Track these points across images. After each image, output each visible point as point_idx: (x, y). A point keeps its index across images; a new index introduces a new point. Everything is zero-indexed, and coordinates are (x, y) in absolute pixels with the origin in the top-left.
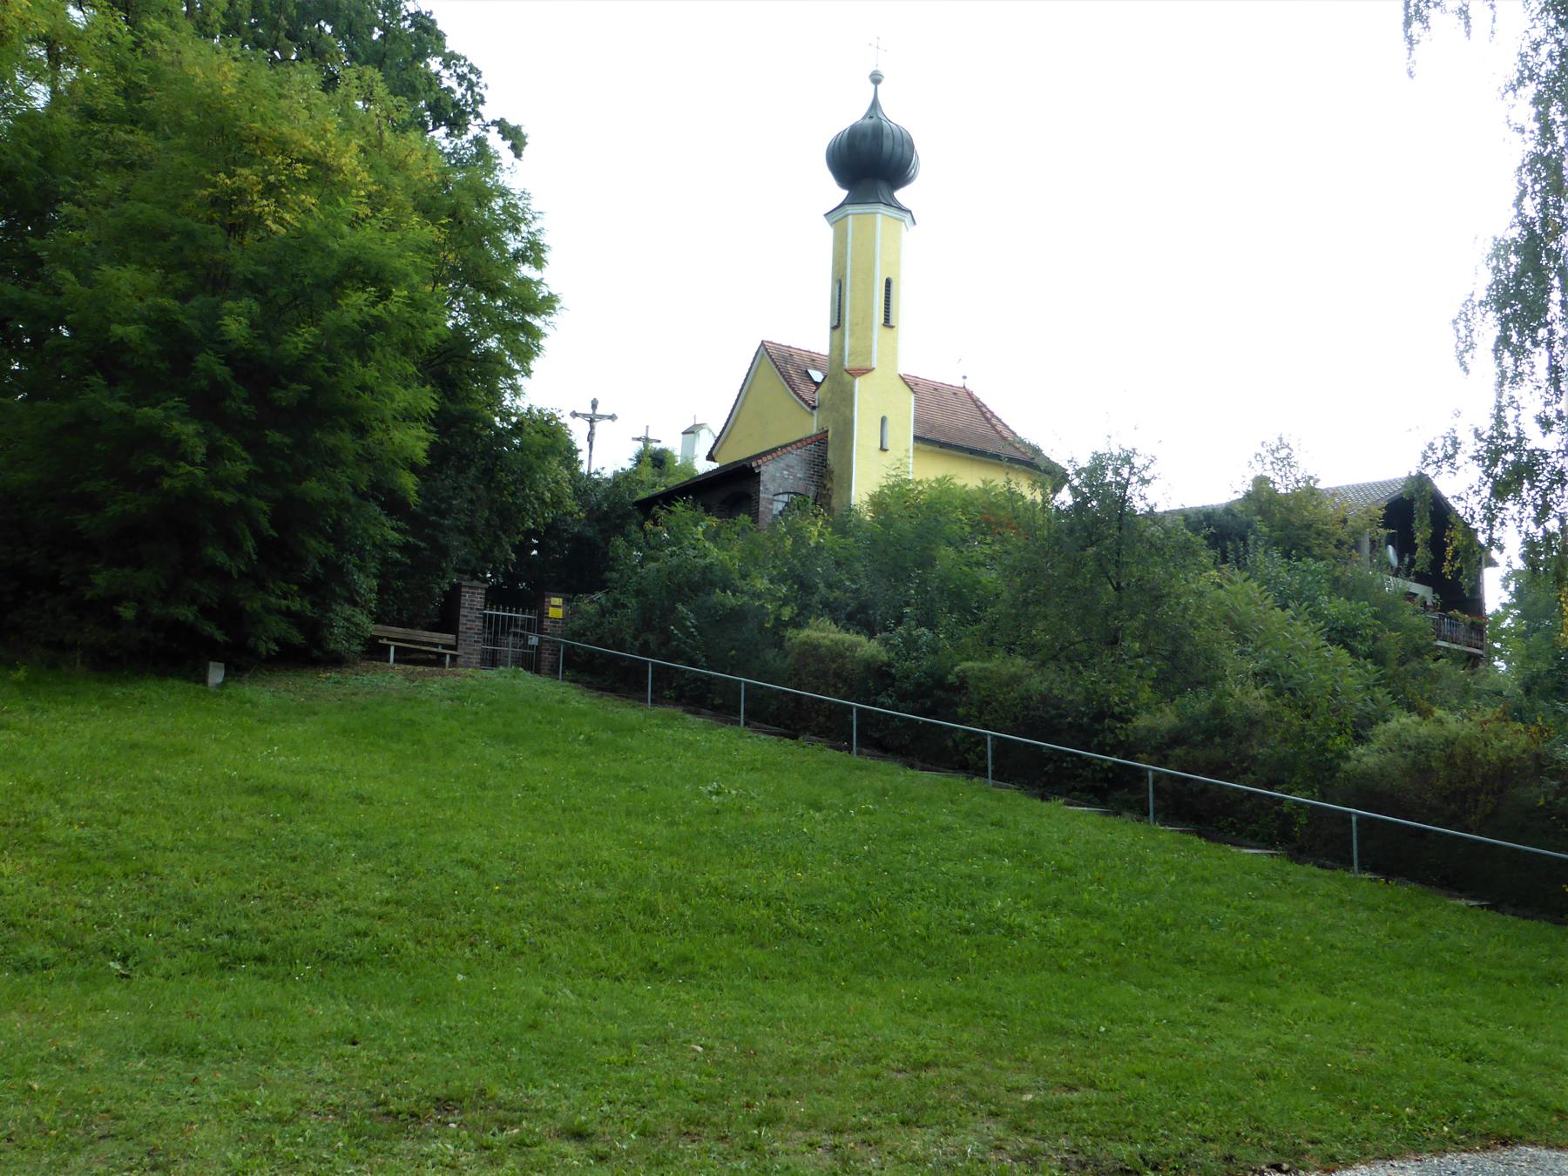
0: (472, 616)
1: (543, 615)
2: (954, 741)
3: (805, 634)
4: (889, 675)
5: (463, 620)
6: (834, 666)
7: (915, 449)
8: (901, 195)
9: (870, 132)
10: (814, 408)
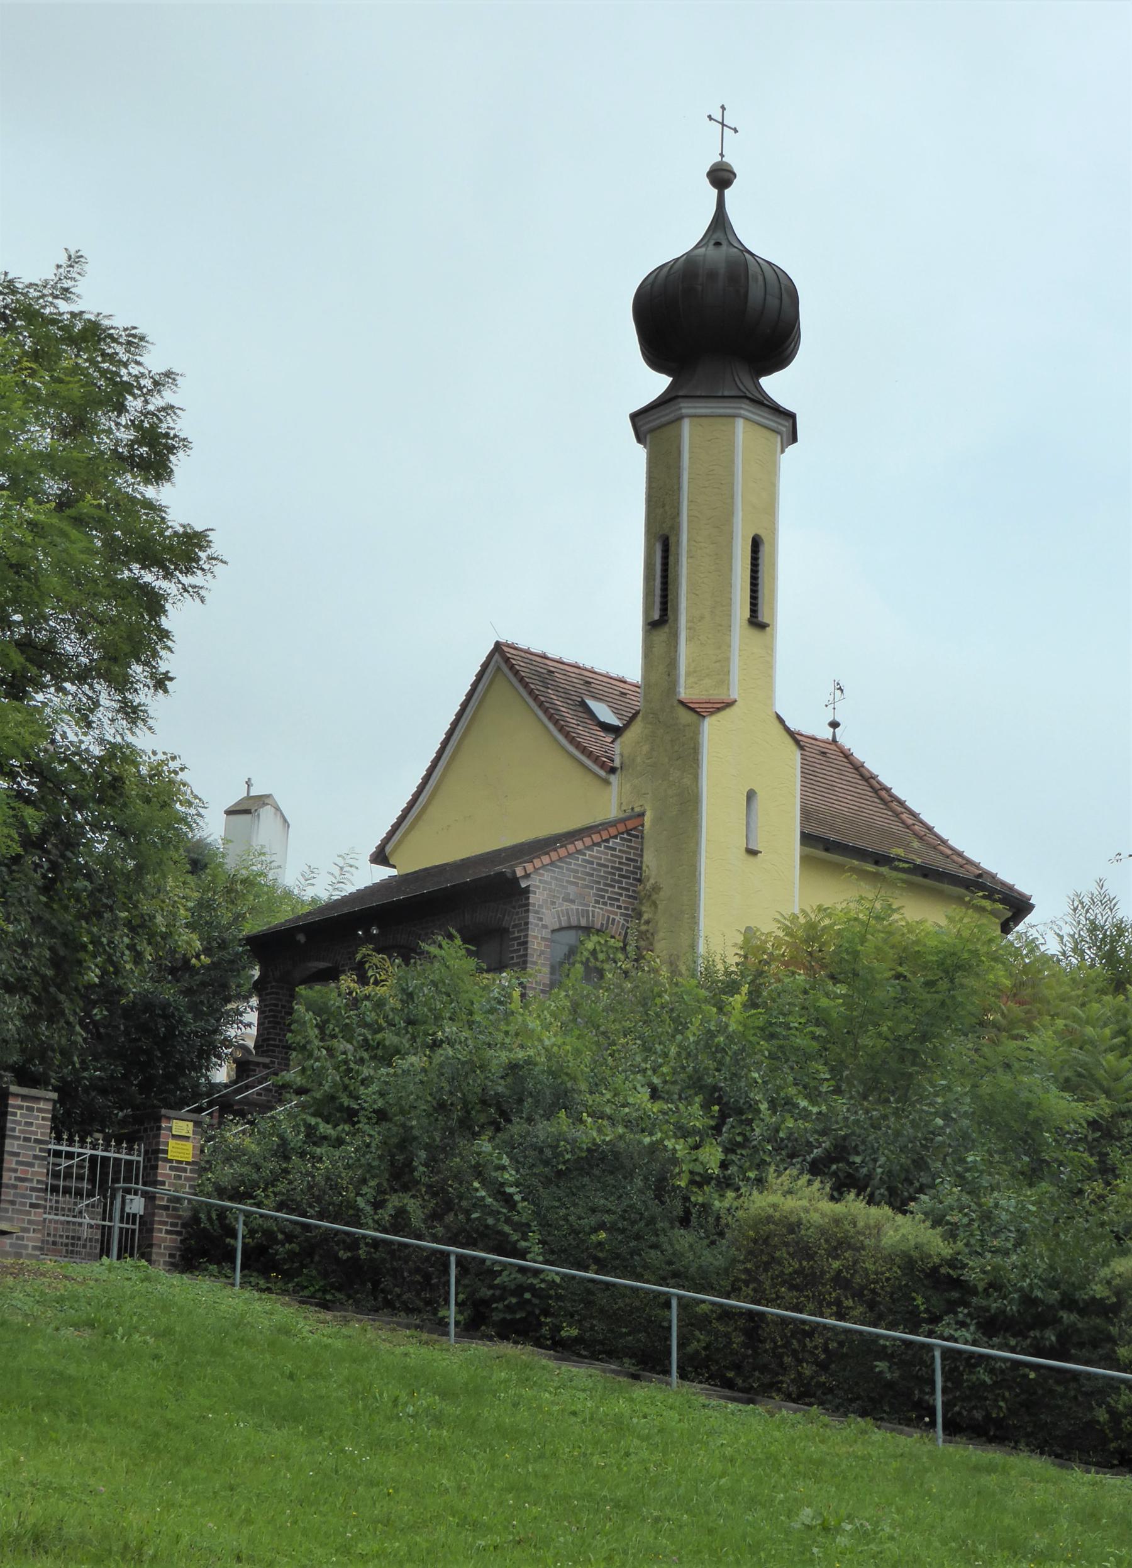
0: (27, 1155)
1: (154, 1155)
2: (1111, 1411)
3: (759, 1202)
4: (957, 1283)
5: (9, 1162)
6: (836, 1264)
7: (805, 860)
8: (773, 385)
9: (722, 271)
10: (613, 770)
